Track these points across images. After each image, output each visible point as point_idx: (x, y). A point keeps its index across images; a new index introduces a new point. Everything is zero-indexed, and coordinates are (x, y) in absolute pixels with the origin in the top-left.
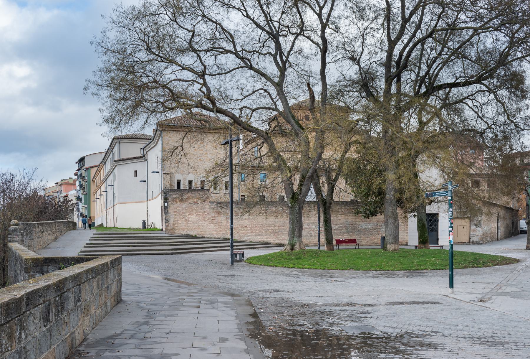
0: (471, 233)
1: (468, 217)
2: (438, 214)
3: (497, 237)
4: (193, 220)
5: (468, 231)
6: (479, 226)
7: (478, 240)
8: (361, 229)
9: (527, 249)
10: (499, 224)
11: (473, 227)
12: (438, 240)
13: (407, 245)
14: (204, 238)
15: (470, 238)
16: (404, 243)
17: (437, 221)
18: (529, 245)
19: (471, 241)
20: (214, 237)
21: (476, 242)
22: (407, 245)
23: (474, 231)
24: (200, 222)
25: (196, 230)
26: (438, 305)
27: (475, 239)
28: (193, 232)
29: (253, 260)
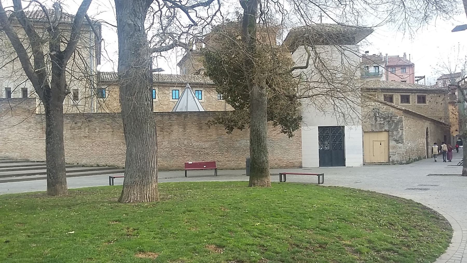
0: (390, 151)
1: (385, 131)
2: (343, 127)
3: (426, 154)
4: (13, 139)
5: (387, 148)
6: (400, 141)
7: (399, 159)
8: (239, 147)
9: (463, 175)
10: (429, 139)
11: (393, 143)
12: (344, 160)
13: (301, 167)
14: (28, 161)
15: (389, 157)
16: (296, 164)
17: (322, 153)
18: (465, 169)
19: (391, 160)
20: (42, 160)
21: (397, 161)
22: (301, 167)
23: (394, 147)
24: (23, 141)
25: (17, 151)
26: (427, 191)
27: (395, 158)
28: (13, 154)
29: (155, 70)
